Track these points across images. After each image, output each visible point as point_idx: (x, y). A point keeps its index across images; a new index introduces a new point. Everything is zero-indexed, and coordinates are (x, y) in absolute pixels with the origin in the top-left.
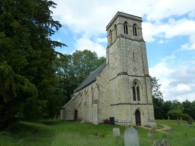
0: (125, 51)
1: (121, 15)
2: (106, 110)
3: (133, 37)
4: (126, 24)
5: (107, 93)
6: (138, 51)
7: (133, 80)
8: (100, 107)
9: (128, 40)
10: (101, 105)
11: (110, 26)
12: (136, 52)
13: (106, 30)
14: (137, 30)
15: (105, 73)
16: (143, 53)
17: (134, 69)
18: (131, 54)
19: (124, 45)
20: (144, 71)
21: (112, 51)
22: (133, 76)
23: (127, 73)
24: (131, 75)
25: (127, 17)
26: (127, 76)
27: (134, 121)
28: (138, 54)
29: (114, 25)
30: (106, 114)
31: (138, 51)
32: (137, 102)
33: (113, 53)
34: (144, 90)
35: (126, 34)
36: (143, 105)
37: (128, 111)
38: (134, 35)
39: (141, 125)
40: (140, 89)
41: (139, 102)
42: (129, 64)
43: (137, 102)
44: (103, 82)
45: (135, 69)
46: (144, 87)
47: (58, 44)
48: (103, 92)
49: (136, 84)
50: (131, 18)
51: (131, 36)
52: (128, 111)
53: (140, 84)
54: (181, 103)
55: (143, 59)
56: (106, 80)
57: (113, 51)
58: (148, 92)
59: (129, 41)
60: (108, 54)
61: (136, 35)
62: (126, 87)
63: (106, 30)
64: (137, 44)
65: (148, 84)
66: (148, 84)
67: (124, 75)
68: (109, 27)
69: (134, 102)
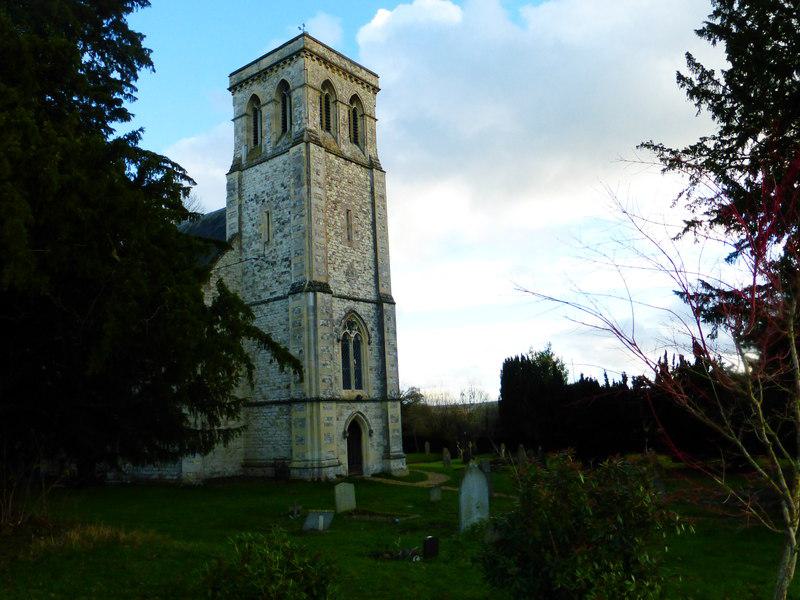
3: (348, 148)
7: (344, 313)
9: (332, 157)
13: (230, 89)
16: (377, 216)
21: (259, 188)
23: (327, 285)
26: (327, 297)
27: (344, 459)
28: (361, 216)
32: (354, 393)
43: (354, 393)
45: (350, 273)
47: (731, 367)
54: (572, 379)
57: (268, 189)
60: (240, 197)
63: (230, 89)
67: (319, 295)
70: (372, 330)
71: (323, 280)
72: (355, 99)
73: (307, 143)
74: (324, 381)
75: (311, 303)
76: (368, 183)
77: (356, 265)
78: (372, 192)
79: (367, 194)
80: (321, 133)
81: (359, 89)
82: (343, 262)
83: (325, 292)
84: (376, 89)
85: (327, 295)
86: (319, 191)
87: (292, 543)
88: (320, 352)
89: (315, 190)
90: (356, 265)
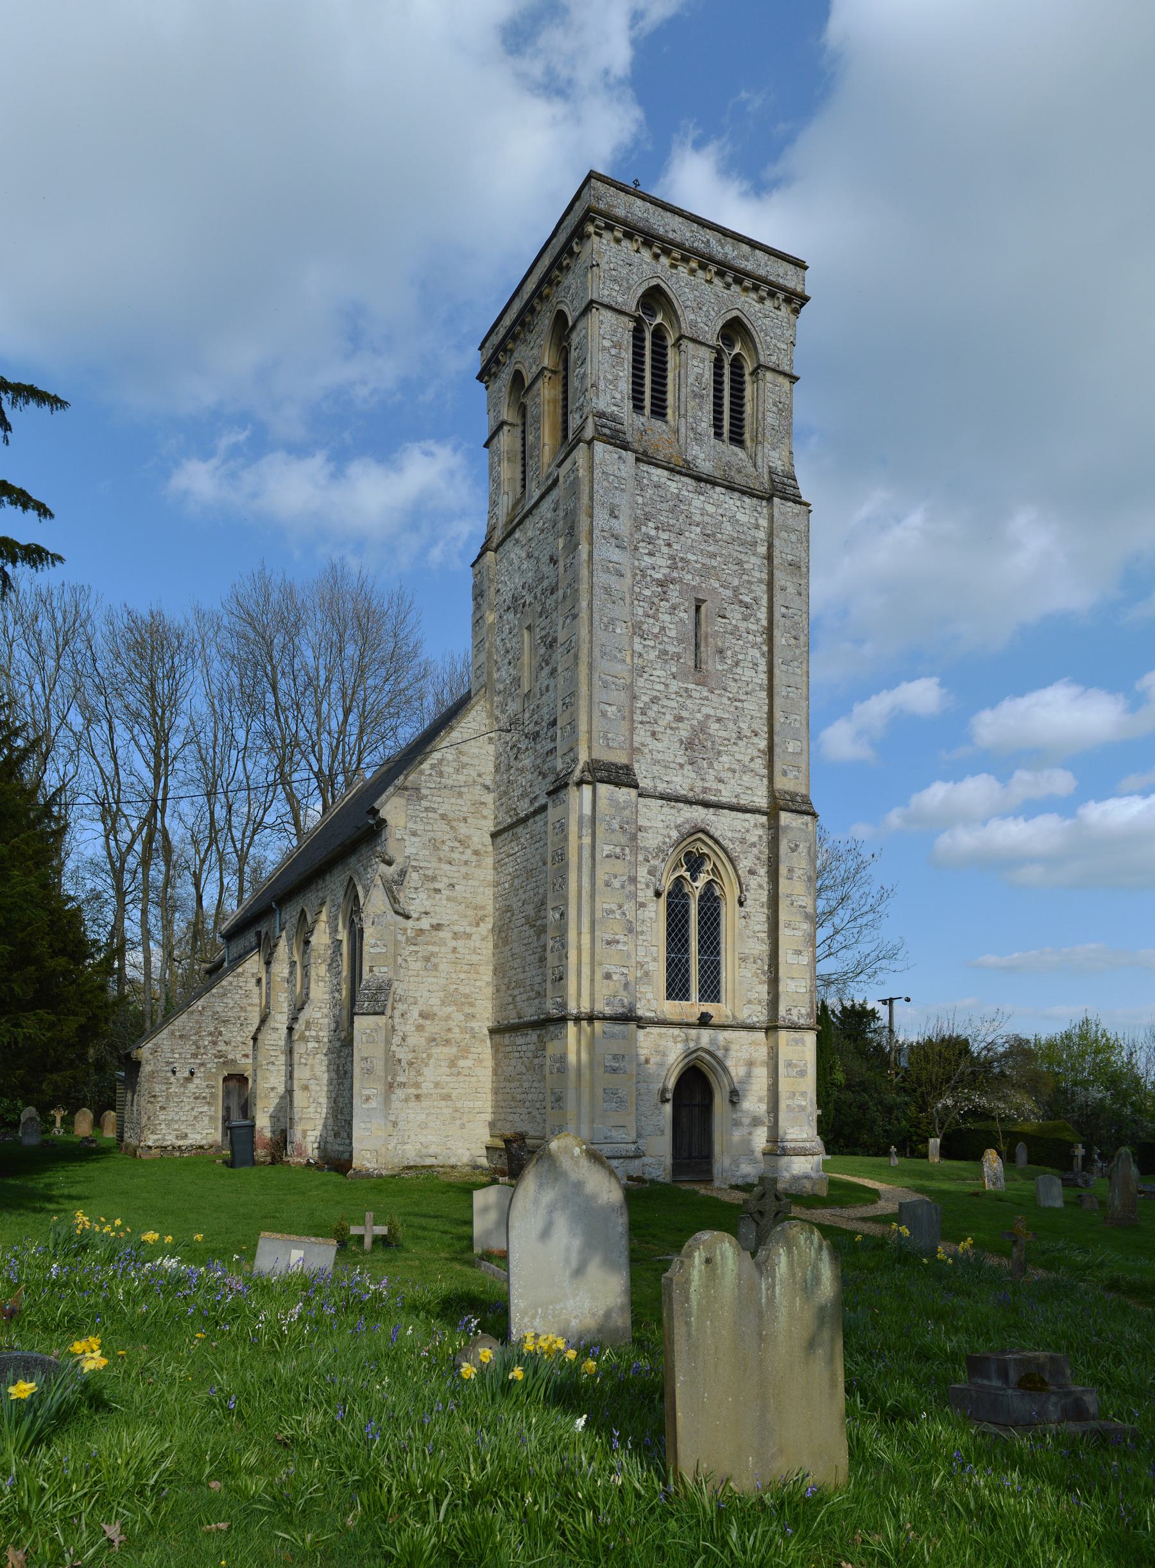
0: (628, 580)
1: (620, 212)
2: (452, 1064)
4: (731, 346)
5: (468, 936)
6: (736, 590)
7: (675, 834)
8: (411, 1041)
10: (420, 1028)
11: (512, 335)
12: (716, 590)
13: (480, 377)
14: (671, 356)
15: (457, 771)
16: (779, 611)
17: (689, 745)
18: (674, 608)
19: (623, 526)
20: (770, 766)
22: (677, 799)
23: (628, 769)
24: (661, 787)
25: (739, 277)
26: (625, 794)
28: (735, 614)
29: (544, 322)
30: (454, 1094)
31: (736, 590)
32: (693, 1007)
33: (529, 599)
34: (759, 918)
35: (643, 420)
36: (743, 1034)
37: (614, 1070)
38: (718, 435)
39: (709, 1180)
40: (729, 914)
41: (709, 1007)
42: (655, 700)
44: (435, 845)
46: (758, 895)
48: (437, 927)
49: (695, 863)
50: (706, 261)
51: (699, 438)
52: (614, 1070)
53: (726, 870)
55: (777, 661)
56: (463, 829)
58: (784, 933)
59: (673, 487)
61: (737, 438)
62: (616, 883)
63: (480, 377)
64: (733, 520)
65: (790, 870)
66: (790, 870)
67: (603, 789)
68: (502, 347)
69: (671, 1009)
70: (752, 872)
71: (621, 758)
72: (734, 329)
73: (590, 443)
74: (608, 976)
75: (587, 810)
76: (761, 535)
77: (714, 726)
78: (770, 557)
79: (754, 562)
80: (632, 422)
81: (748, 305)
82: (679, 719)
83: (618, 784)
84: (796, 300)
85: (624, 790)
86: (616, 555)
87: (240, 1452)
88: (763, 871)
89: (607, 552)
90: (714, 726)
